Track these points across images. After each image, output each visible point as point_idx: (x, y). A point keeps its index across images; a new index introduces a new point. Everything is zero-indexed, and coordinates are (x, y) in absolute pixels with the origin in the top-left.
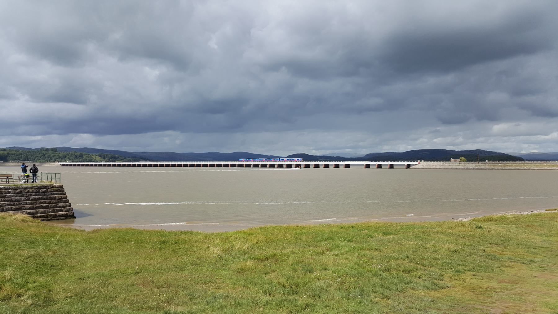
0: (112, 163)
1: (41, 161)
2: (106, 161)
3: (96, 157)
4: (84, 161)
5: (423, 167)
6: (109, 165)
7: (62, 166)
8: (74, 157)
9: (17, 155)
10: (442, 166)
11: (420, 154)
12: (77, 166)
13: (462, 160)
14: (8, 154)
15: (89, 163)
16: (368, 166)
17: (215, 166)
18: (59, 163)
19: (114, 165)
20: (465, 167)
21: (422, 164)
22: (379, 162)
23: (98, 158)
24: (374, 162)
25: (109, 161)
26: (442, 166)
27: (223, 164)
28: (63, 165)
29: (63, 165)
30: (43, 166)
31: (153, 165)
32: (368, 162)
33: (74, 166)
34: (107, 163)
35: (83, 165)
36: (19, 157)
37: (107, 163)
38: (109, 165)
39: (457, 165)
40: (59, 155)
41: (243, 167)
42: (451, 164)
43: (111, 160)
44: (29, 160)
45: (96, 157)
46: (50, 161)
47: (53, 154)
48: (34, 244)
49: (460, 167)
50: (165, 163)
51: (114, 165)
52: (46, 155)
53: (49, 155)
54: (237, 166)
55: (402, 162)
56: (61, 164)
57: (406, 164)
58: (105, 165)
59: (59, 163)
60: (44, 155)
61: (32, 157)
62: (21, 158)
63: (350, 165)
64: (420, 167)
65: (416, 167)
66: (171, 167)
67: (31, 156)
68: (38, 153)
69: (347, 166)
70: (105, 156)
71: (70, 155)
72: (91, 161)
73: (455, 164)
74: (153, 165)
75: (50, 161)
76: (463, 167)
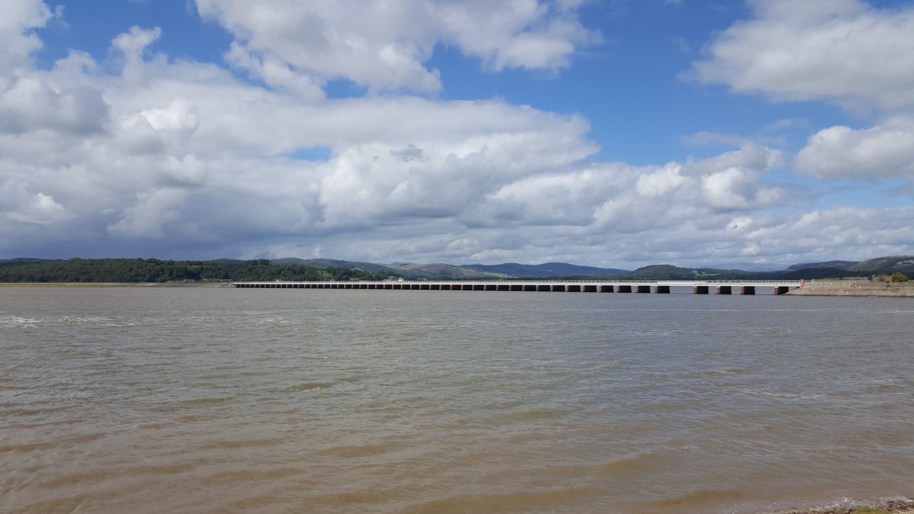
0: (345, 283)
1: (246, 279)
2: (336, 280)
3: (322, 273)
4: (304, 280)
5: (810, 293)
6: (341, 287)
7: (237, 287)
8: (291, 272)
9: (214, 271)
10: (849, 290)
11: (898, 265)
12: (332, 288)
13: (895, 278)
14: (202, 269)
15: (376, 283)
16: (703, 290)
17: (485, 289)
18: (233, 283)
19: (349, 287)
20: (900, 293)
21: (813, 285)
22: (641, 283)
23: (326, 274)
24: (623, 283)
25: (339, 280)
26: (849, 290)
27: (473, 285)
28: (238, 286)
29: (238, 286)
30: (789, 295)
31: (384, 286)
32: (703, 284)
33: (266, 287)
34: (338, 283)
35: (263, 286)
36: (216, 274)
37: (338, 283)
38: (341, 287)
39: (881, 290)
40: (271, 271)
41: (564, 290)
42: (867, 288)
43: (343, 277)
44: (230, 277)
45: (322, 273)
46: (257, 279)
47: (262, 269)
48: (870, 387)
49: (888, 293)
50: (430, 283)
51: (349, 287)
52: (254, 271)
53: (257, 270)
54: (551, 290)
55: (711, 282)
56: (235, 285)
57: (719, 286)
58: (334, 287)
59: (233, 283)
60: (251, 270)
61: (234, 274)
62: (219, 274)
63: (789, 288)
64: (803, 293)
65: (796, 292)
66: (412, 289)
67: (233, 272)
68: (243, 268)
69: (749, 291)
70: (336, 270)
71: (286, 270)
72: (315, 280)
73: (877, 287)
74: (384, 286)
75: (257, 279)
76: (893, 294)
